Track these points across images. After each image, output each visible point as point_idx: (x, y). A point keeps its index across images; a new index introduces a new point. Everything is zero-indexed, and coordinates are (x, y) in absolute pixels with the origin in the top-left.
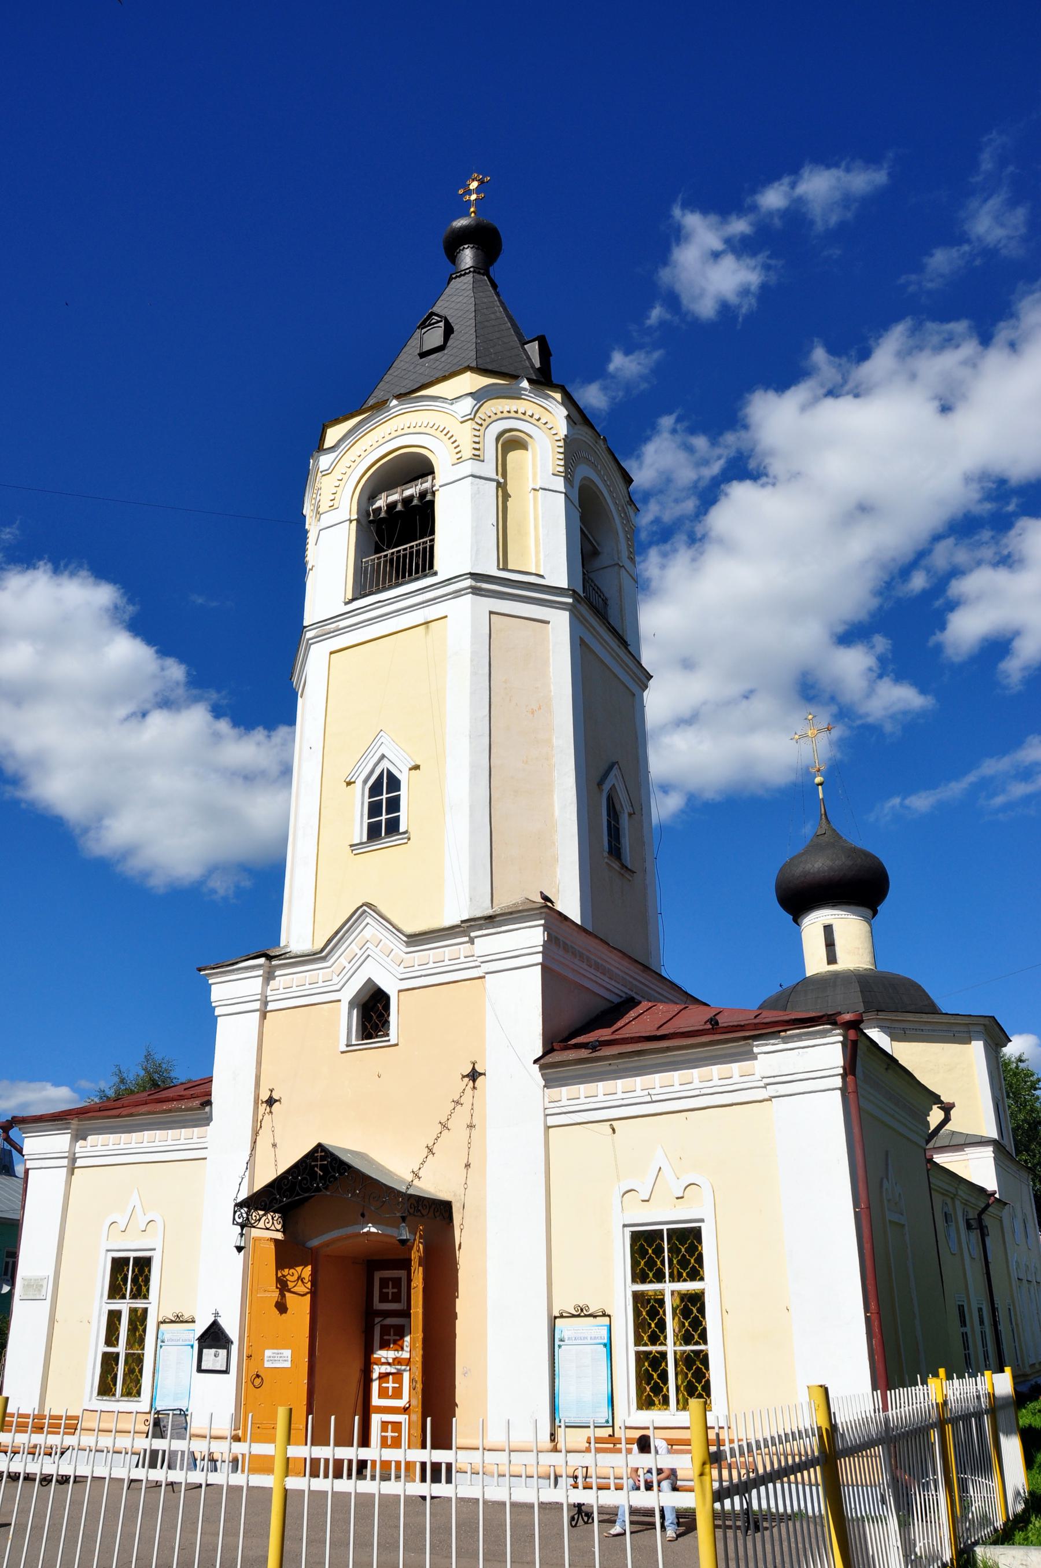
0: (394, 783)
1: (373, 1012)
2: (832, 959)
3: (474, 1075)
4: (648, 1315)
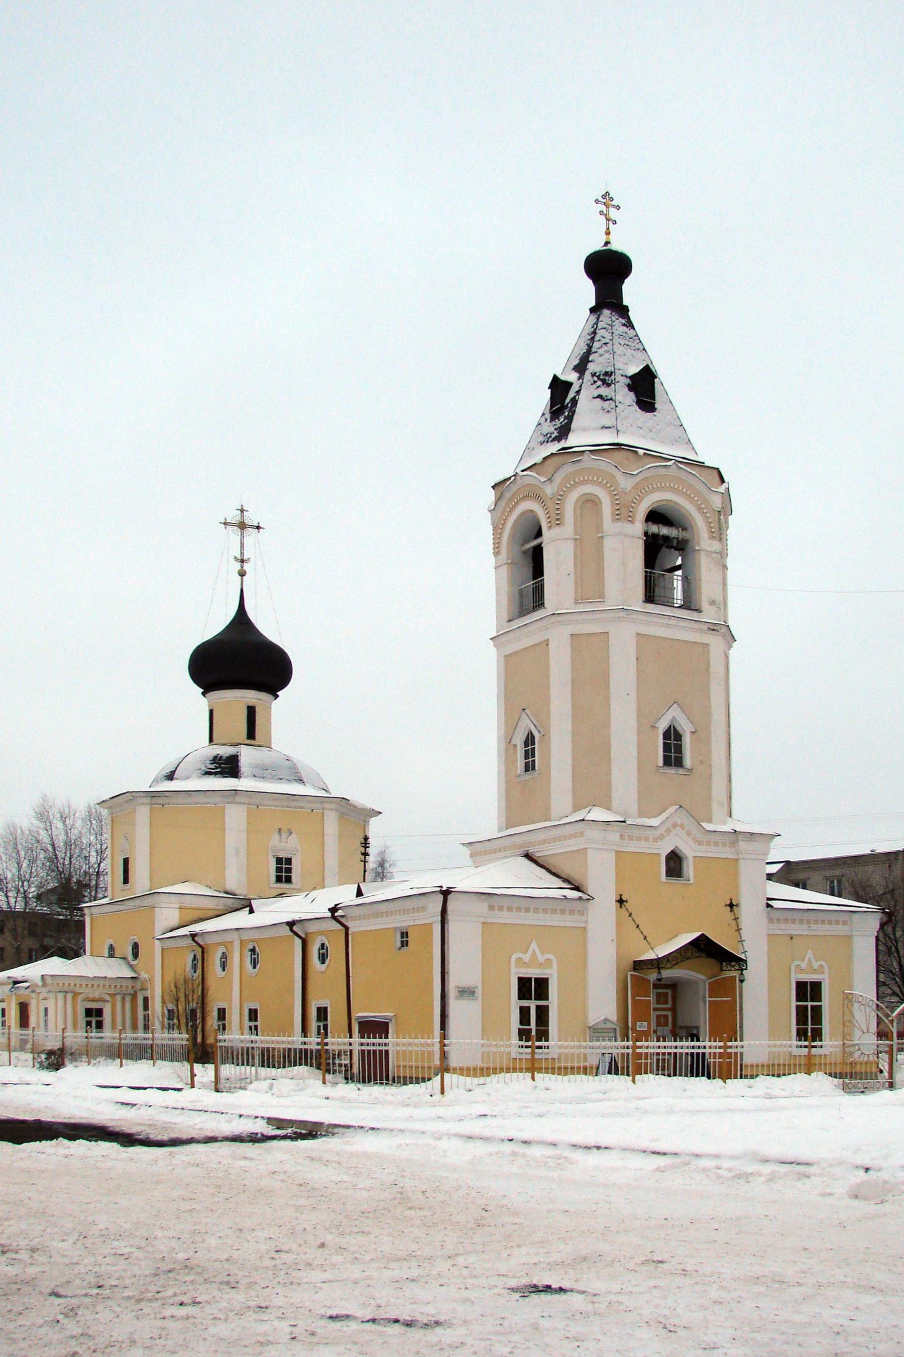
0: (678, 737)
4: (801, 1013)
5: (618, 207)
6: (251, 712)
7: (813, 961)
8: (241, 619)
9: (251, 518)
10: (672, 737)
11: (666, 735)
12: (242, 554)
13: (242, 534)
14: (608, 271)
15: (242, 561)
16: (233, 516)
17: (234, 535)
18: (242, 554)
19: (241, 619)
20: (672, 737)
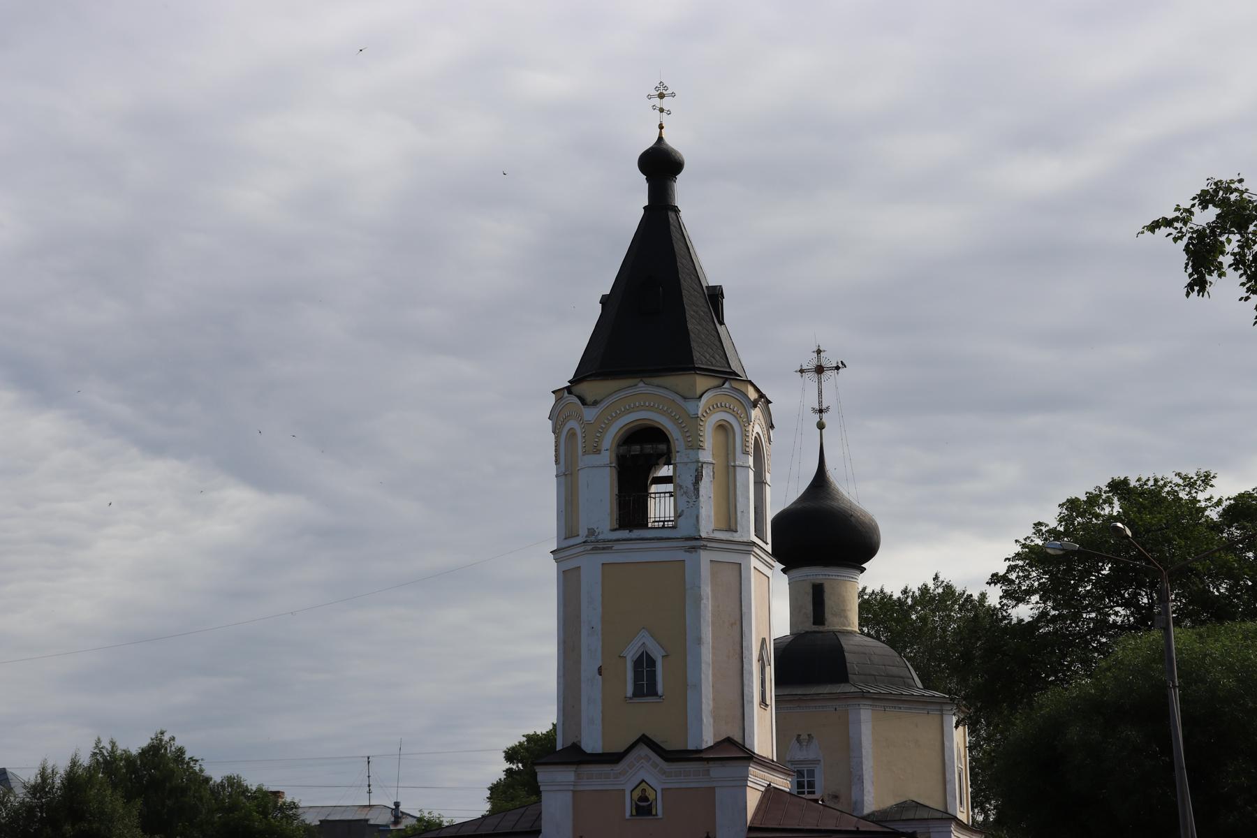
0: (652, 662)
1: (643, 808)
5: (673, 95)
6: (818, 593)
8: (820, 480)
9: (829, 359)
10: (644, 665)
11: (638, 663)
12: (820, 403)
13: (820, 382)
14: (660, 165)
15: (821, 411)
16: (810, 361)
17: (811, 380)
18: (820, 403)
19: (820, 480)
20: (644, 665)
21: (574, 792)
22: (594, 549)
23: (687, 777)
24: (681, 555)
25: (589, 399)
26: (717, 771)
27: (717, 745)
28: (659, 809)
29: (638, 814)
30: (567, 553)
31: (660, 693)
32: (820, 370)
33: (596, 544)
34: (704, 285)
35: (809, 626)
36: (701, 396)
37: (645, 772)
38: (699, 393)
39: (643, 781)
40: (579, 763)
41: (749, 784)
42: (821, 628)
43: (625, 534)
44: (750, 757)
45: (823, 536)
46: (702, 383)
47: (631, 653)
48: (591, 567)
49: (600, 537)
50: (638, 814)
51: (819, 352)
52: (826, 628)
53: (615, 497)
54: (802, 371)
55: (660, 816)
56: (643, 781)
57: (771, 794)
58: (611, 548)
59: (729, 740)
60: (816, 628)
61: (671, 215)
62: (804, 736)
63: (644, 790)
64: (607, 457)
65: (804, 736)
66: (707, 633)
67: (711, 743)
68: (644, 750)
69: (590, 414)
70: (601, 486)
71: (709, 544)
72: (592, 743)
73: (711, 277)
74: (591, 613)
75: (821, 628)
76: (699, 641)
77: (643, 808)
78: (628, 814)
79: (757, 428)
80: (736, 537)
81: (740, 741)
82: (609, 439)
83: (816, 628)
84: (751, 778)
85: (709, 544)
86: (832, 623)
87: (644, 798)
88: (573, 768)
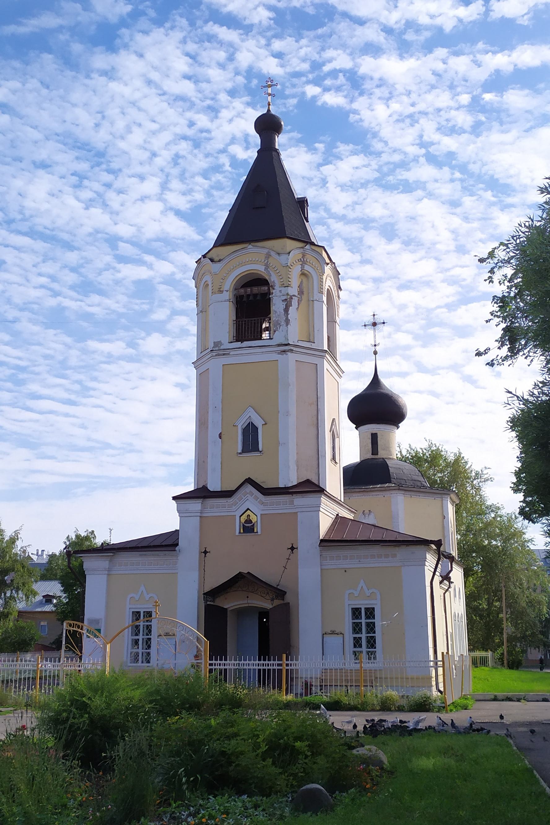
0: (255, 429)
1: (248, 528)
2: (374, 437)
3: (292, 548)
6: (374, 437)
7: (365, 587)
8: (376, 381)
12: (375, 341)
15: (375, 345)
18: (375, 341)
19: (376, 381)
21: (200, 517)
22: (219, 355)
23: (279, 505)
24: (275, 356)
25: (216, 259)
26: (299, 501)
27: (300, 485)
28: (258, 528)
29: (244, 532)
30: (200, 362)
31: (260, 449)
32: (374, 324)
33: (218, 351)
34: (296, 197)
35: (369, 456)
36: (289, 253)
37: (252, 505)
38: (288, 251)
39: (248, 509)
40: (205, 497)
41: (321, 509)
42: (376, 457)
43: (239, 344)
44: (321, 491)
45: (376, 408)
46: (289, 244)
47: (241, 424)
48: (216, 365)
49: (222, 347)
50: (244, 532)
51: (374, 315)
52: (379, 456)
53: (232, 323)
54: (365, 326)
55: (259, 533)
56: (248, 509)
57: (339, 521)
58: (228, 354)
59: (308, 482)
60: (374, 457)
61: (274, 153)
62: (367, 511)
63: (249, 516)
64: (227, 295)
65: (367, 511)
66: (293, 410)
67: (295, 483)
68: (249, 488)
69: (216, 267)
70: (224, 313)
71: (294, 349)
72: (214, 486)
73: (299, 193)
74: (215, 398)
75: (376, 457)
76: (287, 414)
77: (248, 528)
78: (237, 531)
79: (328, 283)
80: (314, 346)
81: (316, 483)
82: (229, 284)
83: (374, 457)
84: (322, 505)
85: (294, 349)
86: (382, 454)
87: (249, 521)
88: (200, 501)
